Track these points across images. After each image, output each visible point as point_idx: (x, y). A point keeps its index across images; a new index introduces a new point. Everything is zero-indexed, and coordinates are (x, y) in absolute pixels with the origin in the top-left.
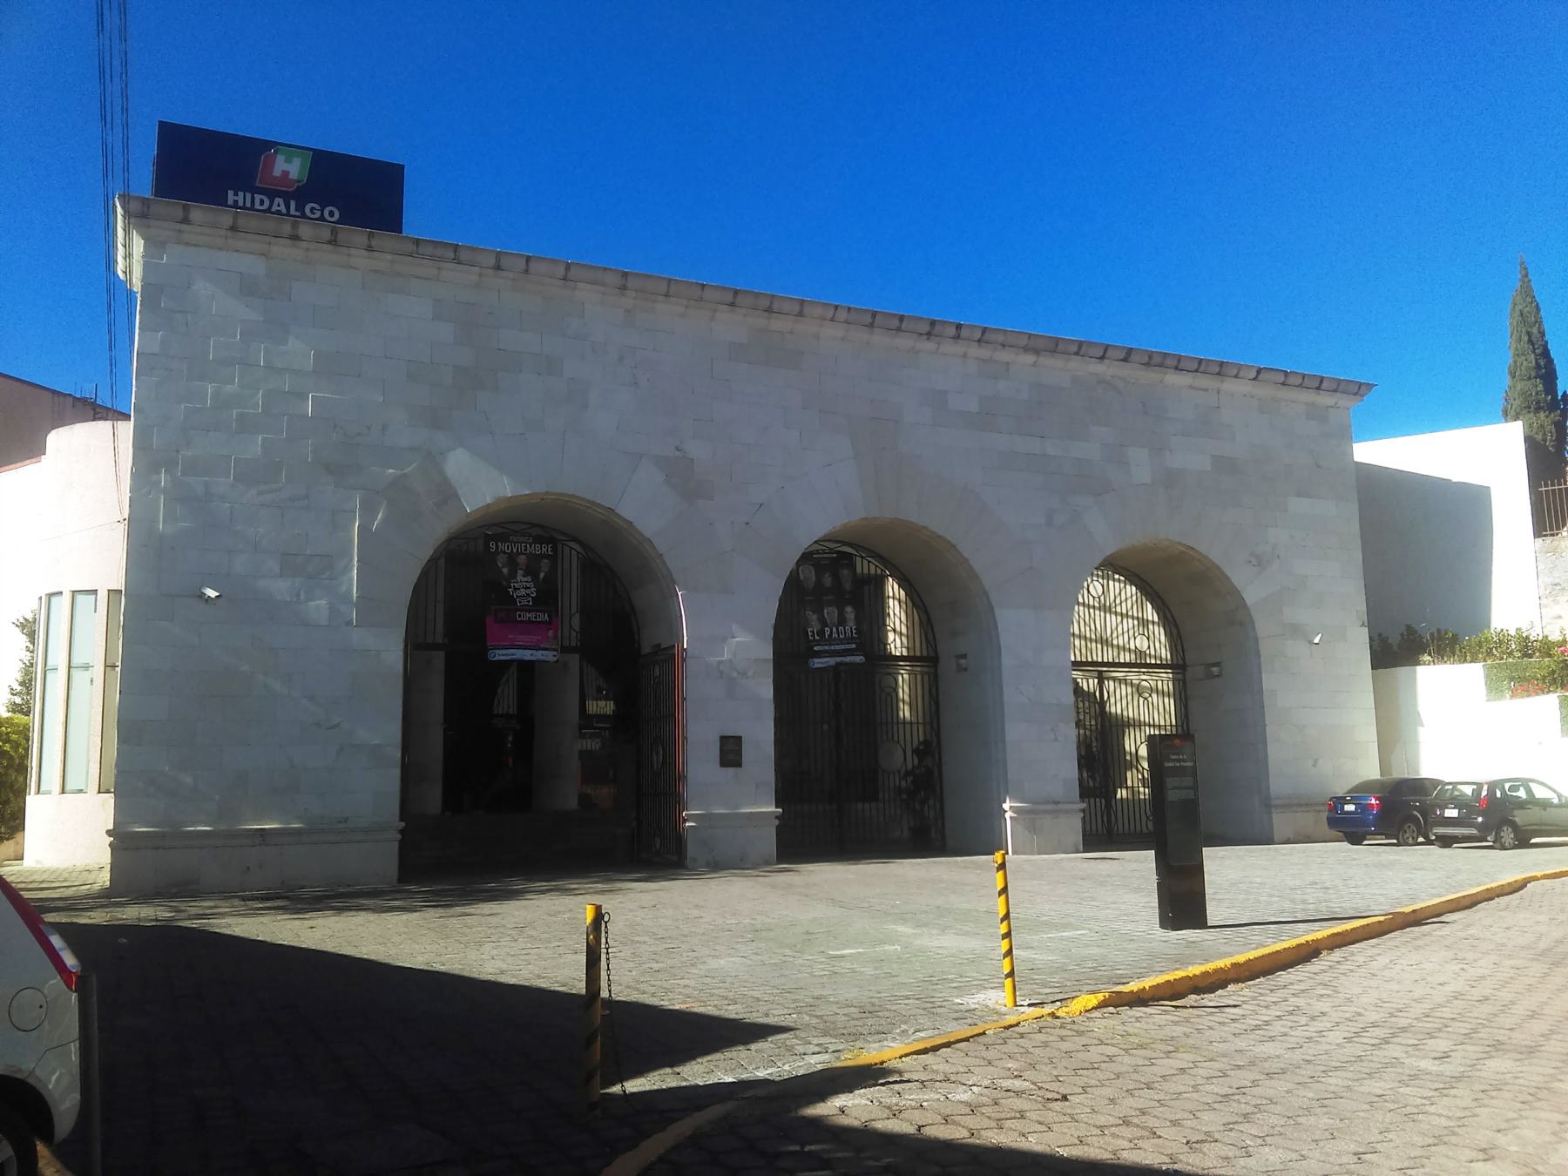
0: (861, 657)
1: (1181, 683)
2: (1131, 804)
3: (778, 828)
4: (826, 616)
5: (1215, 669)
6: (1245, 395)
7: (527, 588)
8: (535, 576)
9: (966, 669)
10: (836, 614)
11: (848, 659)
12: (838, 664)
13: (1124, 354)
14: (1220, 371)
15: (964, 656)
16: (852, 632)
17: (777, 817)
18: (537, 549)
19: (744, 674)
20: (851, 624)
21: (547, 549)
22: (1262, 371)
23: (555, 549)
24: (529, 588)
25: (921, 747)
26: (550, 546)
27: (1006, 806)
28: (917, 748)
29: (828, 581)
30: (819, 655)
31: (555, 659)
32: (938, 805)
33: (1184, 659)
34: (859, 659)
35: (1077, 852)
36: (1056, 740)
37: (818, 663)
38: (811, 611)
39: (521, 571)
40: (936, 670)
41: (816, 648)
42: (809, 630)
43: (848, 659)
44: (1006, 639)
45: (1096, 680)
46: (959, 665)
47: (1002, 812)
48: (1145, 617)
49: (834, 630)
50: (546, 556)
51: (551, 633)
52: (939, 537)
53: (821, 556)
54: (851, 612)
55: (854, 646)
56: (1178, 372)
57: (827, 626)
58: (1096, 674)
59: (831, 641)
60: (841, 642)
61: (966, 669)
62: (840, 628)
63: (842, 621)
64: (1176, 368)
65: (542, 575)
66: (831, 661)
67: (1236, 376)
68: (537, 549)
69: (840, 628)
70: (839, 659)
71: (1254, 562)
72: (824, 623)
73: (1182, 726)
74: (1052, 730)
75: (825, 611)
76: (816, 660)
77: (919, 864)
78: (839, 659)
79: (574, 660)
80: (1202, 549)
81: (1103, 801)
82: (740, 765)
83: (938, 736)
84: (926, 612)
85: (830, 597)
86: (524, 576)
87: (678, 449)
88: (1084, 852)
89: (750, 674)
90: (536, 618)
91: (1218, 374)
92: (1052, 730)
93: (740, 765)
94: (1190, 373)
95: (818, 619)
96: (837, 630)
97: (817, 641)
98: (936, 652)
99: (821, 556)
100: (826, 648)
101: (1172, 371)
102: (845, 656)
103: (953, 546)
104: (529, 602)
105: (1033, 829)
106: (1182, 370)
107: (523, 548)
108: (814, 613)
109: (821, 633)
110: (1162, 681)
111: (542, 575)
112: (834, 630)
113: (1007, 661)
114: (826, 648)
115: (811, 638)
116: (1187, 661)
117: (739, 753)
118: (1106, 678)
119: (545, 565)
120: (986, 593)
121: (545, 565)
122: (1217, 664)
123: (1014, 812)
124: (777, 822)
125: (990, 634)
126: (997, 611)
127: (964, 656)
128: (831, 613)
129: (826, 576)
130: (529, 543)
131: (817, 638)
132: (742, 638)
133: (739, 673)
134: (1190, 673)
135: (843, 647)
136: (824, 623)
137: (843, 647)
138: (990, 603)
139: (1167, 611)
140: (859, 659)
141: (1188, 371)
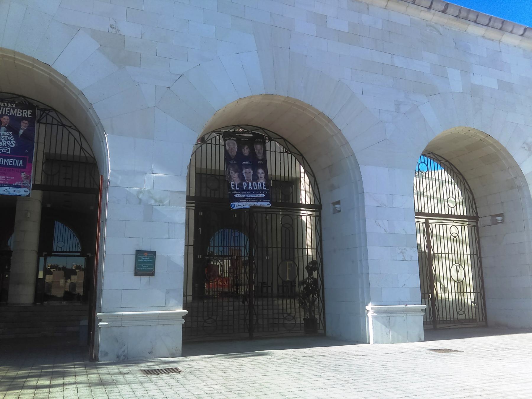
0: (269, 203)
1: (476, 227)
2: (444, 303)
3: (185, 327)
4: (244, 174)
5: (499, 219)
6: (515, 47)
7: (8, 140)
8: (15, 132)
9: (340, 211)
10: (252, 174)
11: (259, 204)
12: (252, 207)
13: (443, 7)
14: (502, 27)
15: (338, 202)
16: (262, 186)
17: (183, 317)
18: (18, 113)
19: (160, 202)
20: (262, 181)
21: (27, 113)
22: (527, 30)
23: (33, 114)
24: (10, 140)
25: (311, 266)
26: (29, 111)
27: (369, 307)
28: (308, 266)
29: (246, 151)
30: (238, 200)
31: (27, 194)
32: (321, 305)
33: (477, 214)
34: (266, 204)
35: (420, 341)
36: (404, 259)
37: (237, 206)
38: (233, 170)
39: (3, 128)
40: (320, 214)
41: (236, 196)
42: (232, 183)
43: (259, 204)
44: (368, 187)
45: (424, 225)
46: (335, 209)
47: (366, 311)
48: (442, 197)
49: (250, 184)
50: (26, 118)
51: (23, 175)
52: (320, 113)
53: (241, 135)
54: (262, 173)
55: (264, 195)
56: (475, 24)
57: (245, 181)
58: (424, 221)
59: (247, 191)
60: (254, 192)
61: (340, 211)
62: (254, 183)
63: (255, 178)
64: (475, 22)
65: (21, 132)
66: (247, 205)
67: (511, 32)
68: (18, 113)
69: (254, 183)
70: (252, 204)
71: (526, 148)
72: (242, 179)
73: (477, 254)
74: (401, 252)
75: (244, 171)
76: (236, 204)
77: (296, 359)
78: (252, 204)
79: (38, 194)
80: (496, 137)
81: (230, 261)
82: (152, 274)
83: (321, 258)
84: (314, 176)
85: (248, 162)
86: (6, 131)
87: (111, 26)
88: (426, 340)
89: (166, 202)
90: (12, 163)
91: (501, 29)
92: (401, 252)
93: (152, 274)
94: (484, 26)
95: (239, 176)
96: (252, 184)
97: (237, 191)
98: (320, 202)
99: (241, 135)
100: (244, 196)
101: (472, 23)
102: (257, 202)
103: (330, 121)
104: (8, 151)
105: (389, 324)
106: (478, 24)
107: (7, 111)
108: (236, 172)
109: (240, 185)
110: (464, 226)
111: (21, 132)
112: (250, 184)
113: (368, 202)
114: (244, 196)
115: (232, 188)
116: (479, 215)
117: (152, 265)
118: (430, 223)
119: (24, 125)
120: (353, 155)
121: (24, 125)
122: (501, 215)
123: (375, 312)
124: (183, 321)
125: (358, 181)
126: (362, 167)
127: (338, 202)
128: (248, 173)
129: (245, 148)
130: (12, 108)
131: (237, 189)
132: (159, 174)
133: (156, 201)
134: (480, 223)
135: (255, 196)
136: (242, 179)
137: (255, 196)
138: (356, 161)
139: (466, 183)
140: (266, 204)
141: (483, 25)
